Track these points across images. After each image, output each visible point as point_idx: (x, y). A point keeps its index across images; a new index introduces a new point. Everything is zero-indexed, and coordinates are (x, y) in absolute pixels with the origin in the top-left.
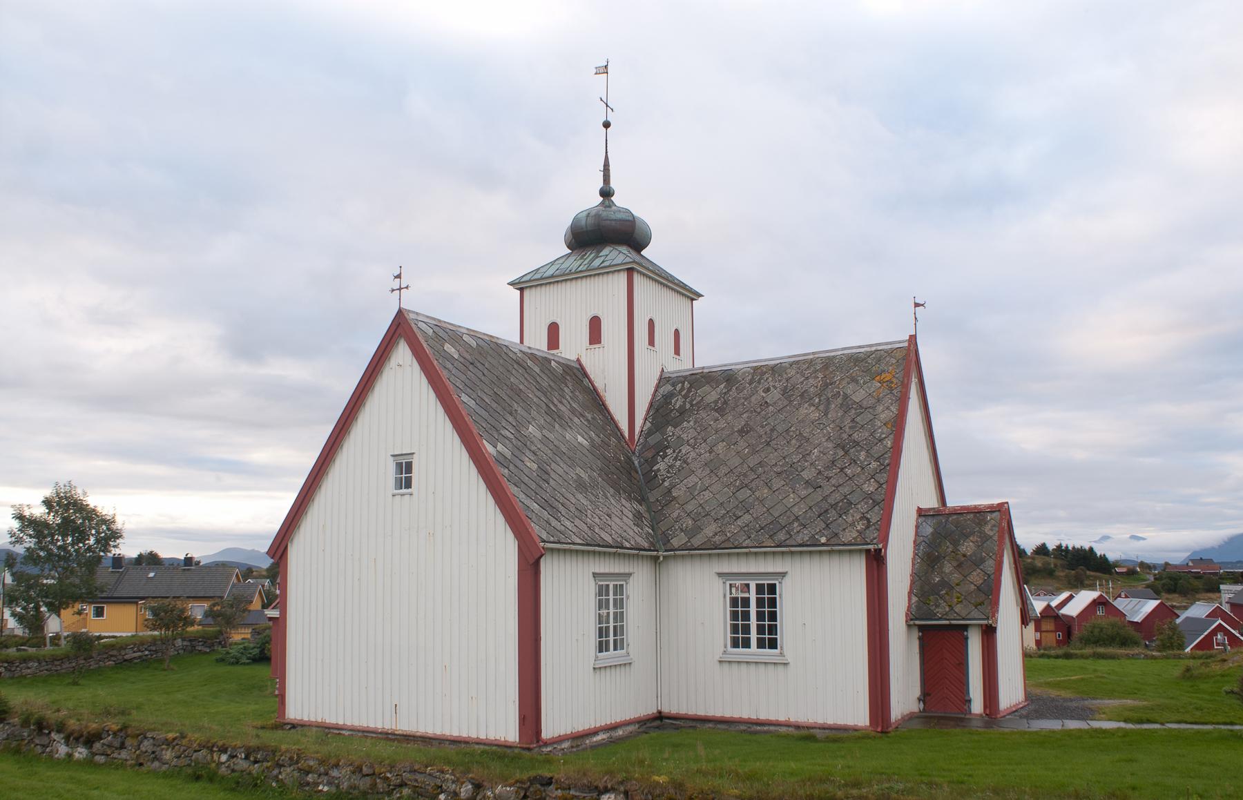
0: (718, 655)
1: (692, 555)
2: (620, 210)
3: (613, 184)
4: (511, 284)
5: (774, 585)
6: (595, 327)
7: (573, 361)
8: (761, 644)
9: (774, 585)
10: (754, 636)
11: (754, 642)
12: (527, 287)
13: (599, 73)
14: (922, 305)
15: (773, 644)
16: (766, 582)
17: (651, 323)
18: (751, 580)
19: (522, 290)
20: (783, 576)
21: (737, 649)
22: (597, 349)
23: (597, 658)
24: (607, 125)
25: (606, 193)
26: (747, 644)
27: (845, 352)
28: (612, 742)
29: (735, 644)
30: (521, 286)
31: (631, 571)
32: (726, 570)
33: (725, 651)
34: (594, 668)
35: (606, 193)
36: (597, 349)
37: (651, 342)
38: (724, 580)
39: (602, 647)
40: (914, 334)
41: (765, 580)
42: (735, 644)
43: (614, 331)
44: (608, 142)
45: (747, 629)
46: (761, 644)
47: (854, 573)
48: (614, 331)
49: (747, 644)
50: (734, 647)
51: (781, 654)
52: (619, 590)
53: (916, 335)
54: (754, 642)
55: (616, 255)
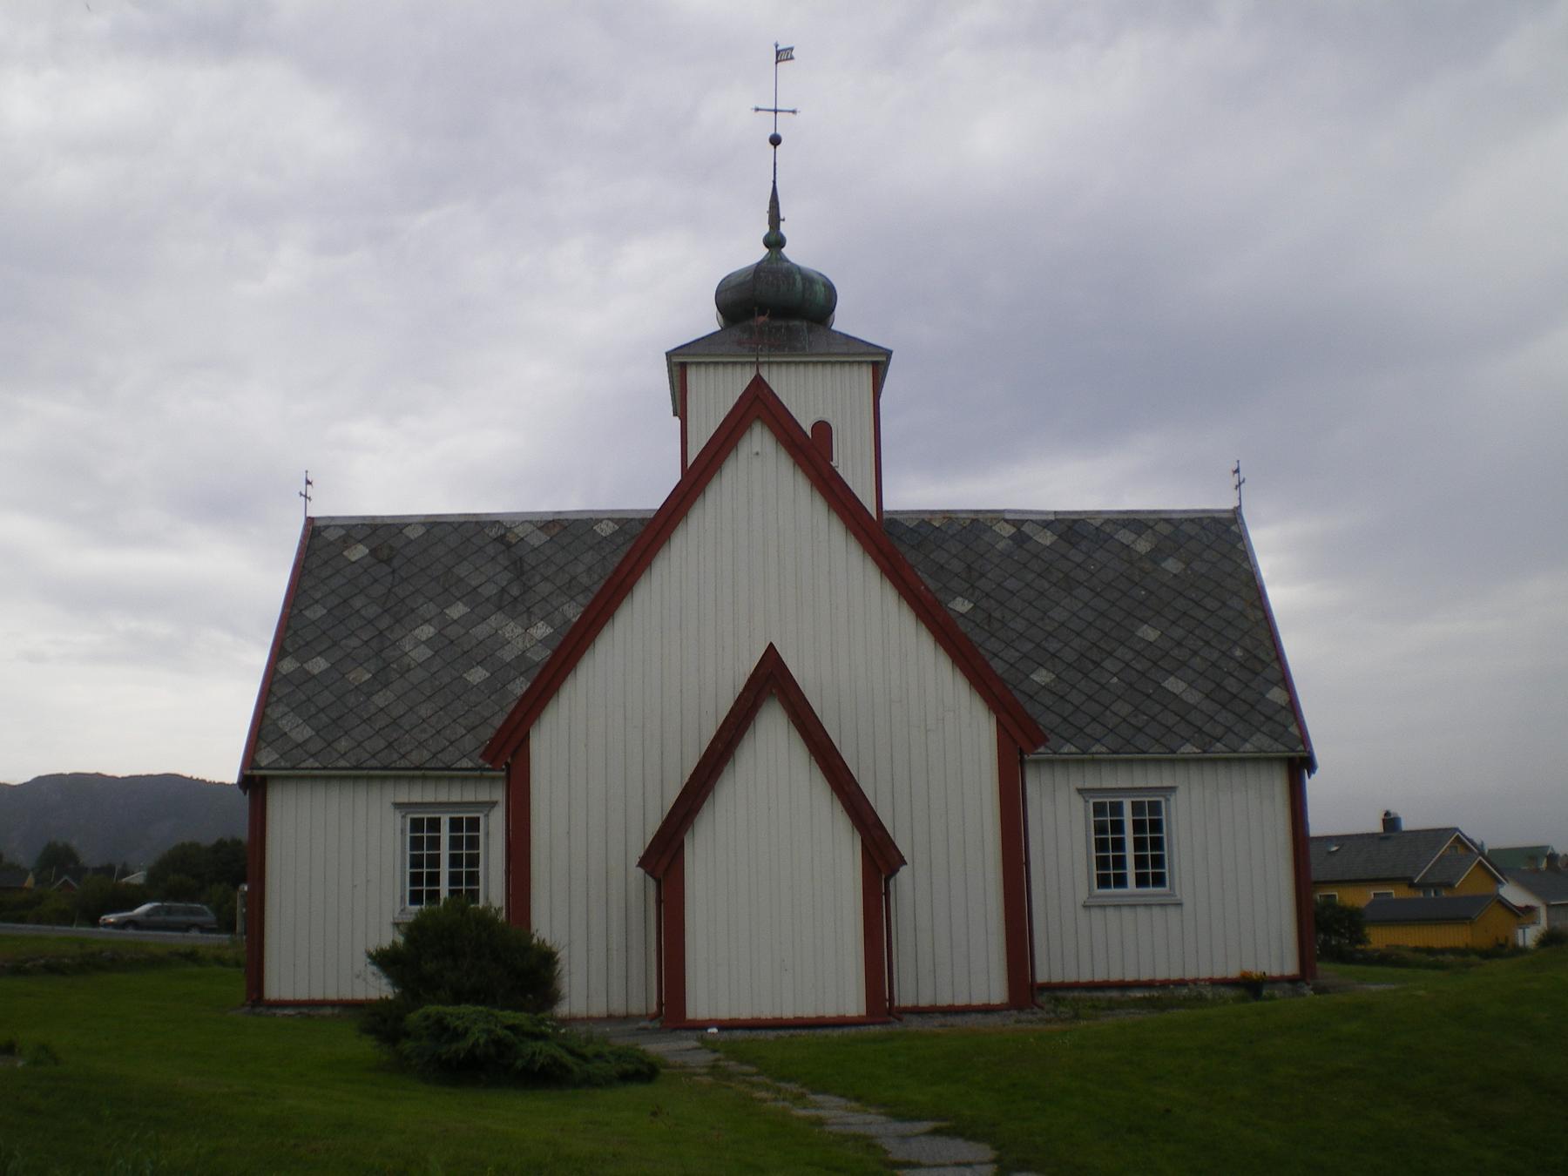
0: (1082, 895)
5: (1159, 803)
8: (1141, 881)
9: (1159, 803)
10: (1131, 871)
12: (692, 363)
15: (1159, 880)
16: (465, 816)
18: (1126, 797)
24: (775, 141)
25: (775, 241)
26: (1121, 881)
29: (1103, 882)
32: (1088, 785)
33: (402, 910)
35: (775, 241)
40: (1237, 504)
41: (1107, 797)
42: (1103, 882)
45: (1120, 862)
46: (1141, 881)
49: (1121, 881)
50: (1126, 884)
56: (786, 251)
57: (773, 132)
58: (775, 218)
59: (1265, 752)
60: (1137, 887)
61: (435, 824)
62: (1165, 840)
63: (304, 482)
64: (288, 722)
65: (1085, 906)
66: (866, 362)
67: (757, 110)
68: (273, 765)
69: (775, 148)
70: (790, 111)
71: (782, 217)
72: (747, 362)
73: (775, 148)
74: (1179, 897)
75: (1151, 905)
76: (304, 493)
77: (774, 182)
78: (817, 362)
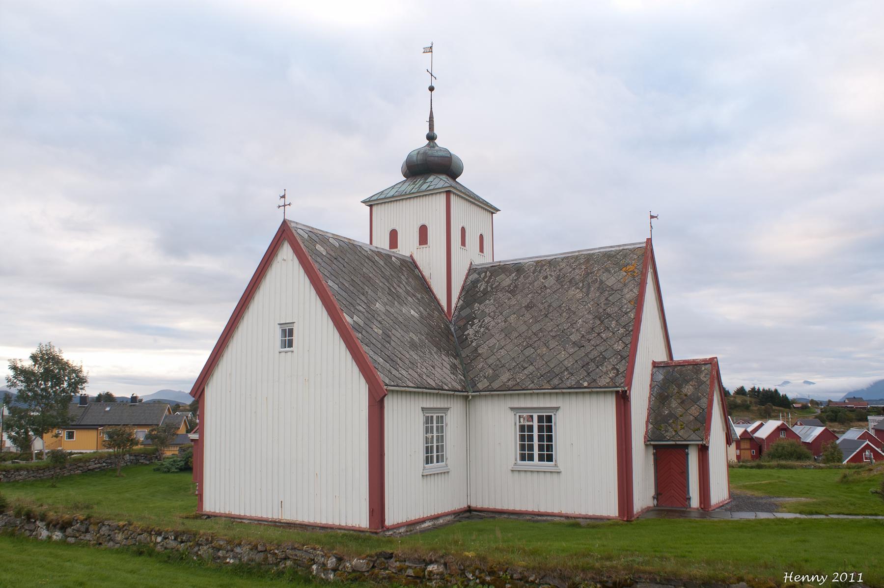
0: (511, 466)
2: (441, 149)
3: (436, 131)
4: (364, 202)
5: (551, 416)
6: (423, 233)
7: (408, 257)
8: (541, 458)
9: (551, 416)
10: (536, 452)
11: (536, 457)
12: (375, 204)
13: (426, 52)
14: (656, 217)
15: (550, 458)
17: (463, 229)
19: (371, 206)
21: (524, 462)
23: (424, 468)
24: (431, 89)
25: (431, 138)
26: (531, 458)
27: (601, 250)
28: (435, 528)
29: (523, 458)
30: (371, 203)
31: (449, 406)
33: (515, 463)
34: (423, 476)
35: (431, 138)
37: (463, 243)
42: (523, 458)
43: (437, 235)
45: (531, 448)
46: (541, 458)
47: (607, 408)
48: (437, 235)
49: (531, 458)
51: (556, 465)
52: (440, 419)
53: (651, 238)
54: (536, 457)
55: (438, 181)
60: (539, 461)
62: (444, 436)
65: (512, 471)
68: (498, 389)
75: (552, 472)
77: (431, 108)
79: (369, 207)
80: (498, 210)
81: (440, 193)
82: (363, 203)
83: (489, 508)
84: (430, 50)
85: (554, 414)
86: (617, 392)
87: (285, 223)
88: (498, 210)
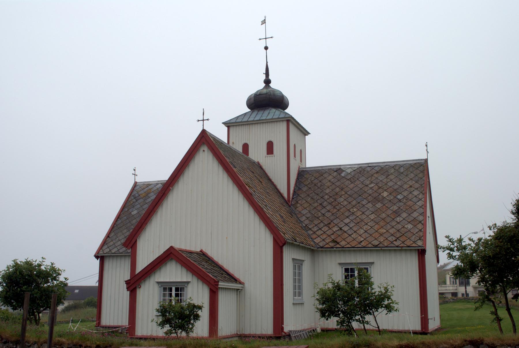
1: (344, 250)
2: (274, 91)
3: (270, 78)
6: (270, 148)
12: (231, 126)
13: (263, 24)
17: (295, 145)
19: (228, 127)
20: (372, 264)
22: (271, 157)
24: (266, 48)
25: (267, 82)
27: (408, 162)
34: (293, 304)
35: (267, 82)
36: (271, 157)
37: (295, 156)
38: (342, 266)
39: (295, 295)
41: (349, 266)
43: (280, 148)
44: (266, 57)
47: (413, 261)
48: (280, 148)
53: (427, 159)
55: (273, 113)
56: (271, 85)
57: (265, 45)
58: (267, 73)
59: (420, 247)
61: (352, 270)
63: (136, 170)
64: (503, 240)
66: (285, 120)
67: (272, 37)
69: (266, 51)
70: (270, 38)
71: (265, 75)
72: (251, 124)
73: (266, 51)
74: (304, 301)
76: (136, 176)
78: (237, 125)
79: (226, 128)
80: (310, 134)
81: (283, 121)
82: (224, 124)
83: (333, 328)
84: (264, 22)
85: (370, 267)
86: (418, 250)
87: (204, 132)
88: (310, 134)
